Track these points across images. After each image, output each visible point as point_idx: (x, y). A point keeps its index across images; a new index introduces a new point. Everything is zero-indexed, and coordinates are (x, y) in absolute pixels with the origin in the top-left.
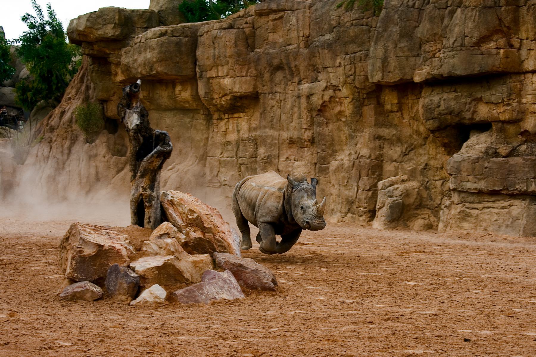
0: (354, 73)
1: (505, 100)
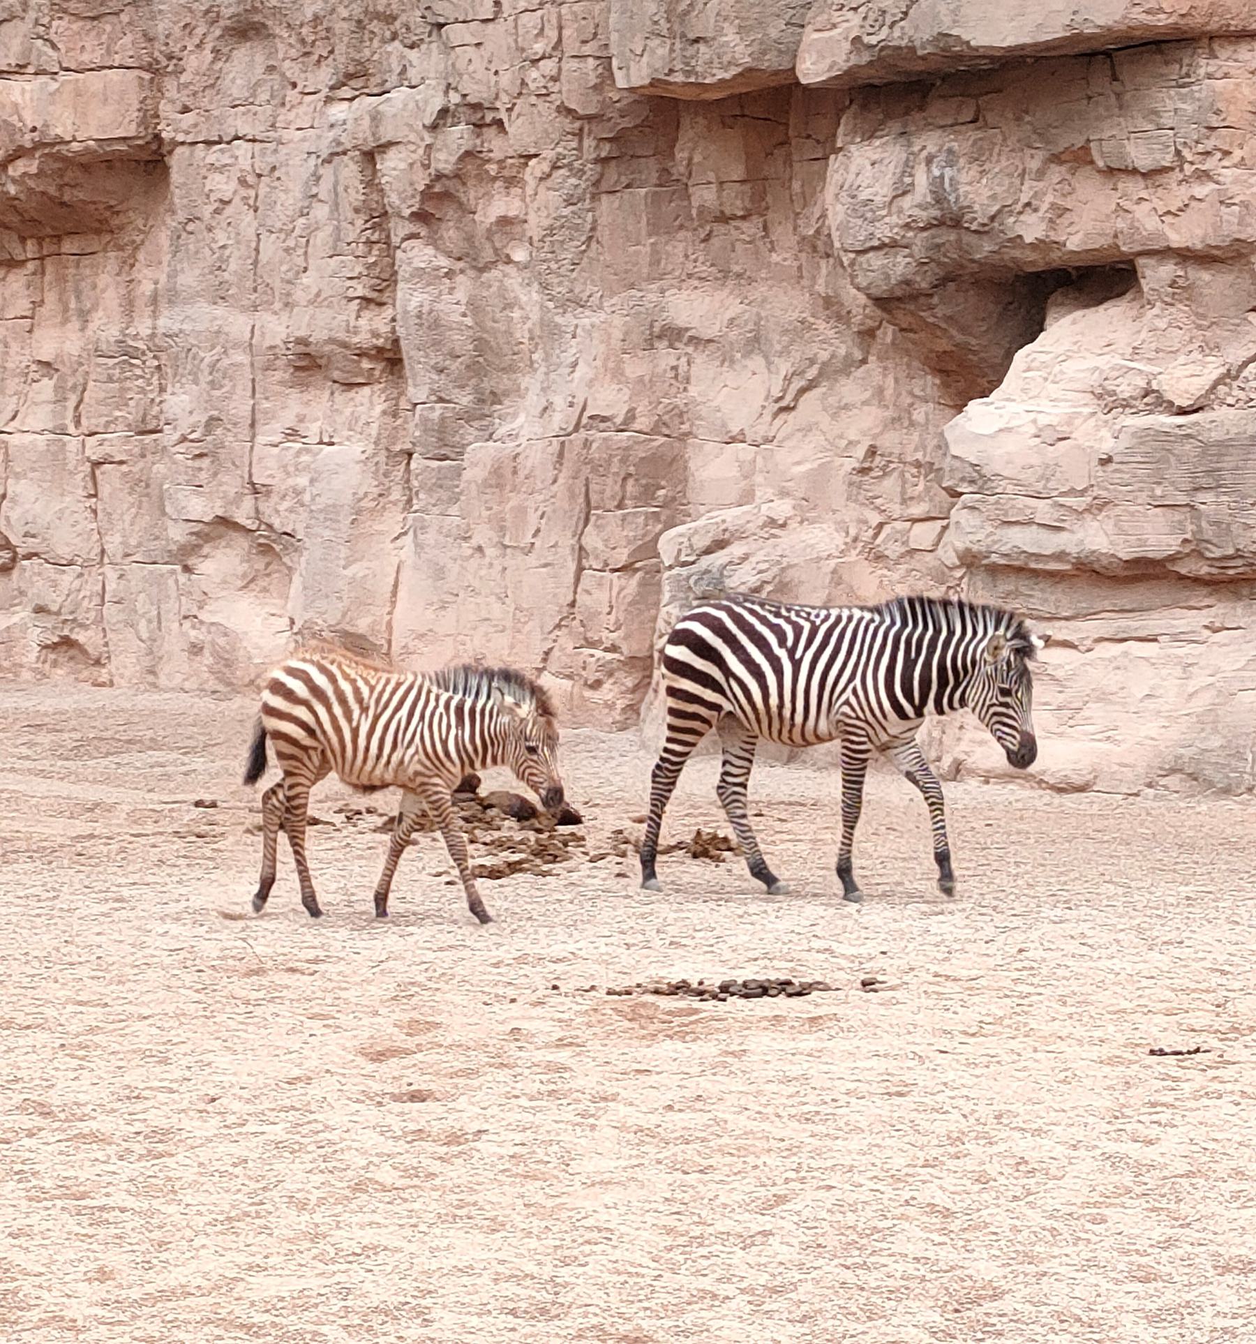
0: (554, 48)
1: (1187, 154)
